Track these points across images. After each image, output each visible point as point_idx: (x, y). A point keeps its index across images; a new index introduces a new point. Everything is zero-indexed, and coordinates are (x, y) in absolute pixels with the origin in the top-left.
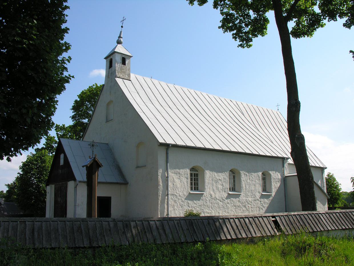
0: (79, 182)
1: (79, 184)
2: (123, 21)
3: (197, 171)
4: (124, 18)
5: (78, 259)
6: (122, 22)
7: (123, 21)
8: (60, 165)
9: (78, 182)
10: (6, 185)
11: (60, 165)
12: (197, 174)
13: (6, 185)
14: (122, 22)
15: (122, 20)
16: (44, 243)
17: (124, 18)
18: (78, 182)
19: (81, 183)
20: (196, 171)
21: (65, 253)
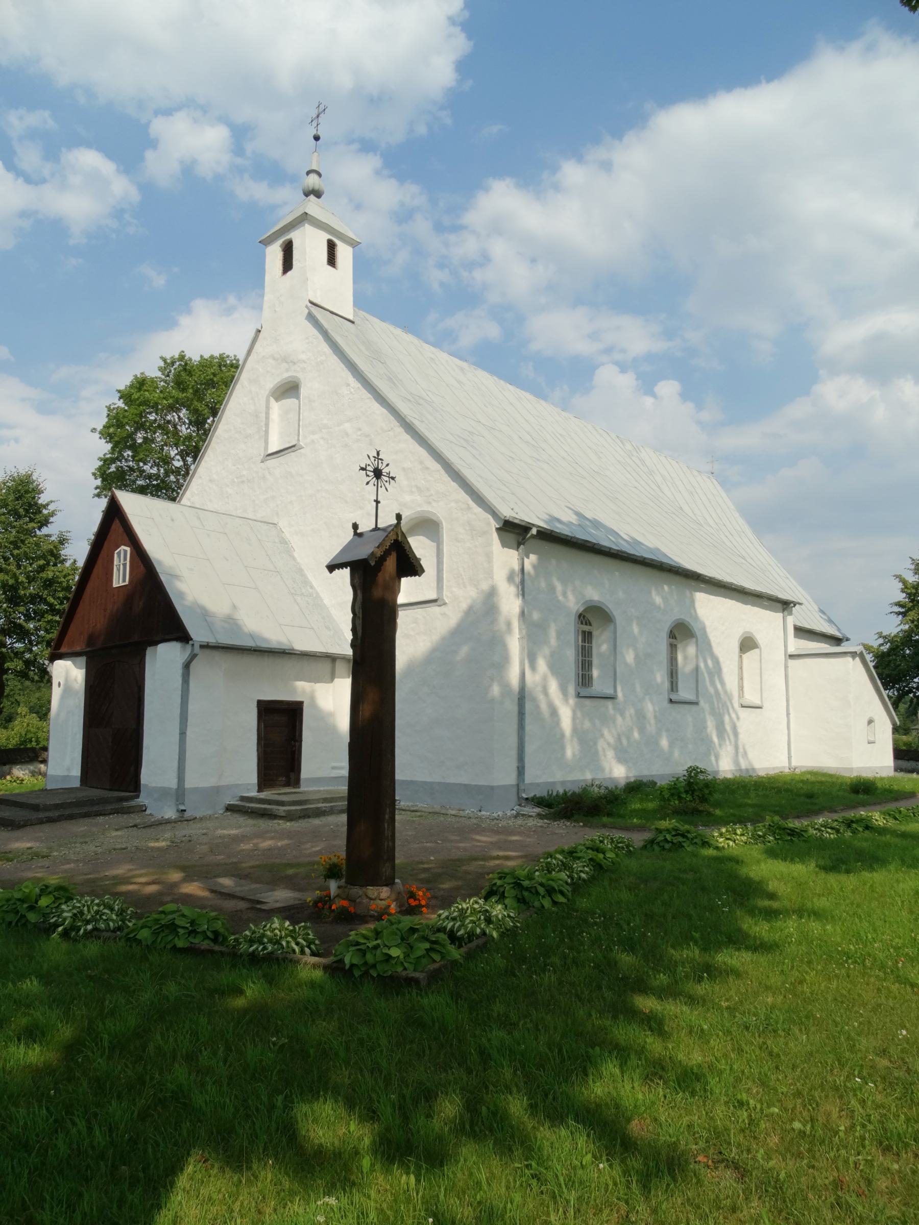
0: (202, 647)
1: (203, 655)
2: (318, 116)
3: (590, 625)
4: (322, 107)
5: (755, 1071)
6: (314, 124)
7: (318, 116)
8: (115, 585)
9: (197, 647)
10: (162, 358)
11: (115, 585)
12: (590, 633)
13: (162, 358)
14: (314, 124)
15: (322, 115)
16: (687, 1118)
17: (322, 107)
18: (197, 649)
19: (207, 651)
20: (586, 624)
21: (898, 1155)
